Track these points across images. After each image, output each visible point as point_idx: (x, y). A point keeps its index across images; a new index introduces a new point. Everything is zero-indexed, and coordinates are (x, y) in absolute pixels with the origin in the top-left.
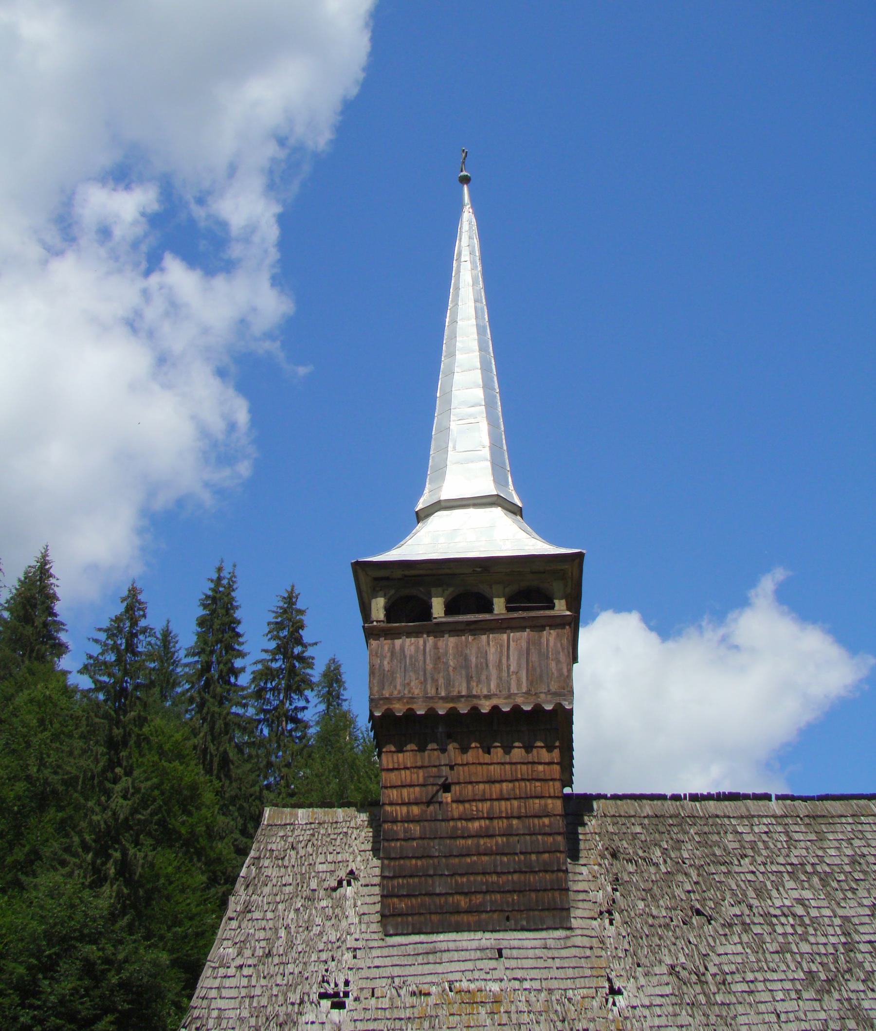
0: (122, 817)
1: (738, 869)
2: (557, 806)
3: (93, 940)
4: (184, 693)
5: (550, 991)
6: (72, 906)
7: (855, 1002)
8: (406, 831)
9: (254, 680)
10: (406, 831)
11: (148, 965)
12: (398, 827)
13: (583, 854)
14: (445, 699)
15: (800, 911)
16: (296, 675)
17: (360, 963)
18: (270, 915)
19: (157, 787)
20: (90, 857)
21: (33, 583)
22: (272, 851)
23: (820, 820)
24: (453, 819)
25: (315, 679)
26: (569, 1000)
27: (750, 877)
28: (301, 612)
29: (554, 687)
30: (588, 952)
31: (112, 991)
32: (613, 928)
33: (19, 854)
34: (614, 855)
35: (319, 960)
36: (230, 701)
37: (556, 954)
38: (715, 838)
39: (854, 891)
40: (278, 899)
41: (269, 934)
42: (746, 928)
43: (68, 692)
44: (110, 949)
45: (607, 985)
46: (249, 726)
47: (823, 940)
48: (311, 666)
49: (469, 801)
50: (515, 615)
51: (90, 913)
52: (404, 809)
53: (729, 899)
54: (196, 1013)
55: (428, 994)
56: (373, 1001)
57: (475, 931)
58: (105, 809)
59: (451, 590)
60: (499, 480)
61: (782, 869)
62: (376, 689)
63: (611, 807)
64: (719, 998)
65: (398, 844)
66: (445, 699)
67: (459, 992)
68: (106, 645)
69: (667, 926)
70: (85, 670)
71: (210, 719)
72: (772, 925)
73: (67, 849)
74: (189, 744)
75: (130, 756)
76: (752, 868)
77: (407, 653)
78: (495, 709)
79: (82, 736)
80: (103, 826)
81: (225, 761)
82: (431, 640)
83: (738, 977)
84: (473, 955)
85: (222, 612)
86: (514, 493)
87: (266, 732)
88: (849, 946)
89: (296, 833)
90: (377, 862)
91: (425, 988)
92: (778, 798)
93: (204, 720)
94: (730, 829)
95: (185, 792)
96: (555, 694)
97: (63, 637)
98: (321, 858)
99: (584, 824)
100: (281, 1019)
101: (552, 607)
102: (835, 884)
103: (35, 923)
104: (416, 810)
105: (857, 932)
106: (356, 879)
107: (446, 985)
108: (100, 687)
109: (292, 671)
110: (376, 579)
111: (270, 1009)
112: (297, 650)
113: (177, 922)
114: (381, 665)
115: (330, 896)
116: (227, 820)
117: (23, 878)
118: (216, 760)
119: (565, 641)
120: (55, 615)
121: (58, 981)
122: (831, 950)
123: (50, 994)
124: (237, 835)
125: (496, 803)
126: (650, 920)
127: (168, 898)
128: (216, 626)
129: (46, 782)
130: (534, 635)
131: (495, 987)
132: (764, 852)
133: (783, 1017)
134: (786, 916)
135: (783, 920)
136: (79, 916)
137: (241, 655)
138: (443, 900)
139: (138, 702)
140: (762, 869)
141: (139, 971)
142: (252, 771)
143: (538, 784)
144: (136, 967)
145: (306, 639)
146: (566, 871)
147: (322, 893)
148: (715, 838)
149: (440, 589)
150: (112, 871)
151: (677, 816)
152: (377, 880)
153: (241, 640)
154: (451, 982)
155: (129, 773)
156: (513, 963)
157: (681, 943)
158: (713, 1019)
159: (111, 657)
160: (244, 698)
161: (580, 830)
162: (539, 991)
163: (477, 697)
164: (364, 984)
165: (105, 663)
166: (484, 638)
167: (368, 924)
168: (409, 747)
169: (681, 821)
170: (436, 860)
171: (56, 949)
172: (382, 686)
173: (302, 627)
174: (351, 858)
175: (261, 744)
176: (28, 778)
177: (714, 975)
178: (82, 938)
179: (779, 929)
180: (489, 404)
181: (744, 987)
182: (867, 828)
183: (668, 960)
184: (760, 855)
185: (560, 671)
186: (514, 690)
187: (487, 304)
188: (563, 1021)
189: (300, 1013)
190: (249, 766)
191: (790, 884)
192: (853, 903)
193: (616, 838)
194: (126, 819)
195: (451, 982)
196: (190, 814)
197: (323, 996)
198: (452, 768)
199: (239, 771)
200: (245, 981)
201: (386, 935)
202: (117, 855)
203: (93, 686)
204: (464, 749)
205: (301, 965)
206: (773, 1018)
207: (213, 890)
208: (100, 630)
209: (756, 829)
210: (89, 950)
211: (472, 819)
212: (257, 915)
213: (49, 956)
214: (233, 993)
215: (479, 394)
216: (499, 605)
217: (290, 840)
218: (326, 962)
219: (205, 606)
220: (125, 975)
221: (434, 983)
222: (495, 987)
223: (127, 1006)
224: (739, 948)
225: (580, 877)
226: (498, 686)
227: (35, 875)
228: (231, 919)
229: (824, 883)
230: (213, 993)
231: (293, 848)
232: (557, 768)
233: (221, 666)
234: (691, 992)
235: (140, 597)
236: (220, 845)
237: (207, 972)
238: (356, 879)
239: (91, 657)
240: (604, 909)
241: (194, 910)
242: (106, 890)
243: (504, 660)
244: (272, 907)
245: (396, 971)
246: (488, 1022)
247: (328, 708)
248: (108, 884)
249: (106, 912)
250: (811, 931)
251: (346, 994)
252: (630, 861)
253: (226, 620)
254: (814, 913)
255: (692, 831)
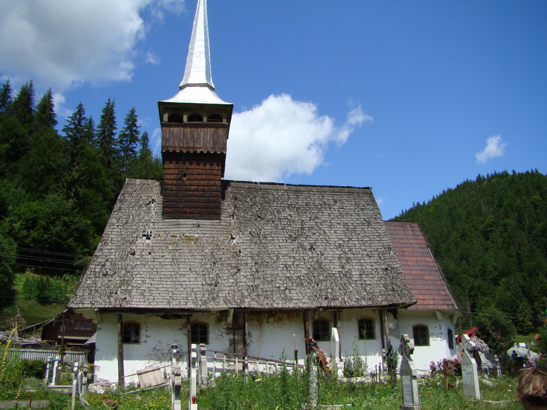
0: (76, 178)
1: (272, 205)
2: (219, 183)
3: (67, 215)
4: (96, 140)
5: (213, 237)
6: (60, 205)
7: (302, 244)
8: (171, 188)
9: (120, 137)
10: (171, 188)
11: (84, 224)
12: (169, 187)
13: (226, 198)
14: (186, 148)
15: (289, 218)
16: (134, 136)
17: (156, 227)
18: (127, 211)
19: (86, 169)
20: (65, 190)
21: (46, 100)
22: (128, 192)
23: (298, 192)
24: (186, 185)
25: (140, 138)
26: (219, 240)
27: (276, 207)
28: (136, 116)
29: (221, 146)
30: (226, 227)
31: (73, 231)
32: (233, 220)
33: (42, 188)
34: (235, 199)
35: (142, 225)
36: (111, 143)
37: (216, 227)
38: (267, 195)
39: (305, 213)
40: (130, 206)
41: (127, 217)
42: (273, 222)
43: (58, 137)
44: (72, 218)
45: (230, 236)
46: (117, 152)
47: (295, 226)
48: (138, 134)
49: (192, 180)
50: (210, 123)
51: (66, 207)
52: (171, 181)
53: (269, 214)
54: (104, 238)
55: (176, 237)
56: (159, 238)
57: (191, 219)
58: (70, 175)
59: (190, 113)
60: (208, 79)
61: (285, 206)
62: (164, 143)
63: (236, 185)
64: (263, 241)
65: (169, 192)
66: (186, 148)
67: (186, 236)
68: (71, 122)
69: (250, 220)
70: (64, 130)
71: (105, 149)
72: (281, 222)
73: (58, 187)
74: (98, 156)
75: (78, 159)
76: (277, 205)
77: (174, 132)
78: (202, 152)
79: (63, 152)
80: (69, 180)
81: (109, 163)
82: (182, 129)
83: (269, 236)
84: (190, 226)
85: (109, 114)
86: (212, 83)
87: (123, 154)
88: (302, 229)
89: (136, 187)
90: (161, 197)
91: (175, 235)
92: (286, 185)
93: (103, 149)
94: (271, 193)
95: (96, 172)
96: (221, 149)
97: (56, 119)
98: (144, 195)
99: (227, 189)
100: (131, 242)
101: (222, 121)
102: (300, 211)
103: (48, 209)
104: (175, 182)
105: (305, 224)
106: (155, 202)
107: (182, 234)
108: (69, 136)
109: (132, 135)
110: (166, 108)
111: (127, 238)
112: (134, 128)
113: (93, 212)
114: (166, 136)
115: (146, 206)
116: (109, 181)
117: (44, 195)
118: (106, 162)
119: (225, 132)
120: (53, 111)
121: (56, 227)
122: (297, 229)
123: (54, 230)
124: (112, 186)
125: (200, 181)
126: (245, 219)
127: (90, 204)
128: (107, 119)
129: (51, 166)
130: (216, 130)
131: (197, 236)
132: (281, 201)
133: (281, 247)
134: (285, 219)
135: (284, 220)
136: (62, 208)
137: (115, 129)
138: (182, 209)
139: (81, 142)
140: (280, 205)
141: (81, 226)
142: (118, 166)
143: (214, 176)
144: (80, 224)
145: (137, 125)
146: (221, 203)
147: (144, 205)
148: (267, 195)
149: (186, 113)
150: (73, 195)
151: (255, 188)
152: (161, 202)
153: (115, 124)
154: (183, 234)
155: (78, 164)
156: (203, 229)
157: (254, 226)
158: (261, 247)
159: (73, 126)
160: (116, 143)
161: (226, 191)
162: (210, 237)
163: (196, 148)
164: (156, 233)
165: (71, 128)
166: (199, 129)
167: (158, 215)
168: (173, 162)
169: (257, 190)
170: (180, 198)
171: (55, 217)
172: (166, 143)
173: (136, 121)
174: (153, 195)
175: (121, 158)
176: (45, 164)
177: (263, 235)
178: (63, 214)
179: (283, 223)
180: (206, 53)
181: (271, 238)
182: (311, 195)
183: (249, 230)
184: (279, 201)
185: (223, 142)
186: (208, 147)
187: (208, 19)
188: (217, 246)
189: (137, 240)
190: (117, 165)
191: (287, 210)
192: (305, 216)
193: (236, 194)
194: (77, 179)
195: (183, 234)
196: (97, 179)
197: (144, 236)
198: (187, 169)
199: (114, 166)
200: (119, 230)
201: (164, 219)
202: (74, 190)
203: (66, 136)
204: (191, 164)
205: (137, 227)
206: (279, 247)
207: (104, 202)
208: (69, 117)
209: (279, 194)
210: (66, 218)
211: (192, 186)
212: (123, 211)
213: (53, 219)
214: (116, 233)
215: (203, 50)
216: (205, 119)
217: (134, 189)
218: (145, 226)
219: (104, 112)
220: (76, 226)
221: (178, 234)
222: (197, 236)
223: (78, 235)
224: (271, 228)
225: (225, 205)
226: (203, 145)
227: (47, 194)
228: (115, 211)
229: (297, 210)
230: (110, 233)
231: (135, 191)
232: (220, 172)
233: (109, 132)
234: (255, 240)
235: (83, 107)
236: (107, 189)
237: (108, 227)
238: (155, 202)
239: (66, 126)
240: (231, 214)
241: (99, 208)
242: (71, 200)
243: (206, 137)
244: (128, 209)
245: (167, 230)
246: (194, 245)
247: (143, 148)
248: (71, 199)
249: (70, 207)
250: (292, 223)
251: (151, 235)
252: (240, 201)
253: (111, 117)
254: (293, 219)
255: (260, 193)
